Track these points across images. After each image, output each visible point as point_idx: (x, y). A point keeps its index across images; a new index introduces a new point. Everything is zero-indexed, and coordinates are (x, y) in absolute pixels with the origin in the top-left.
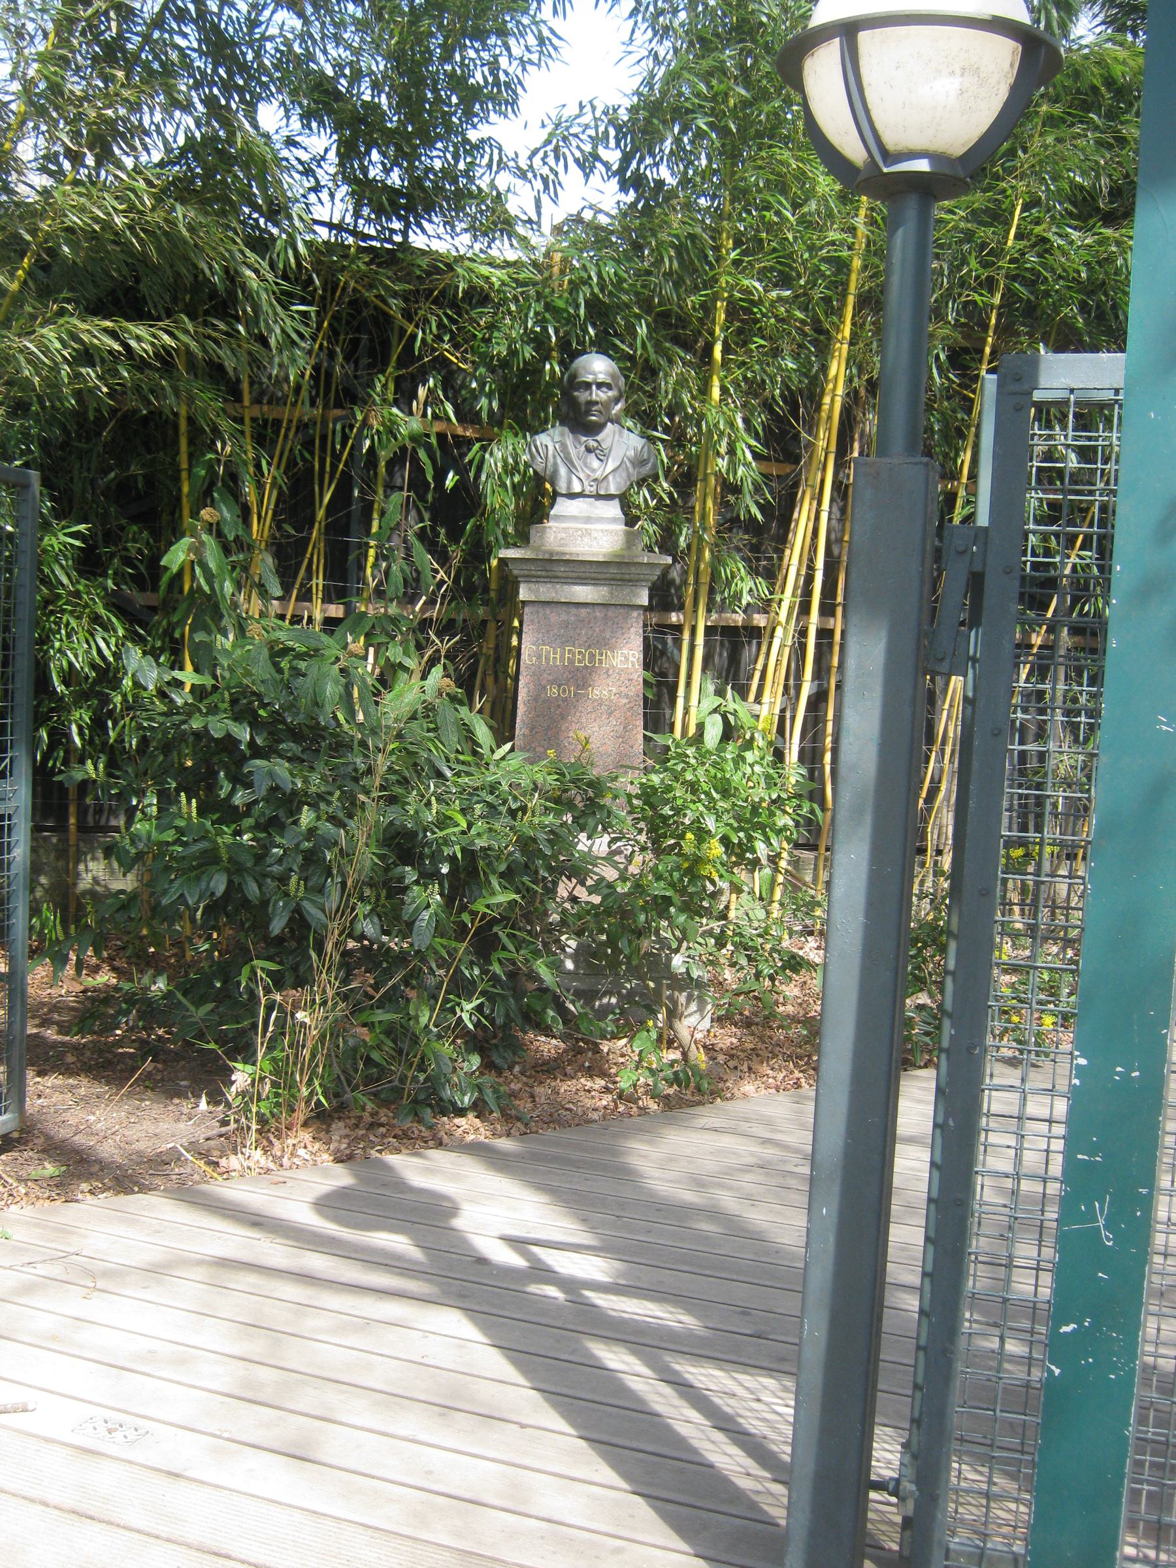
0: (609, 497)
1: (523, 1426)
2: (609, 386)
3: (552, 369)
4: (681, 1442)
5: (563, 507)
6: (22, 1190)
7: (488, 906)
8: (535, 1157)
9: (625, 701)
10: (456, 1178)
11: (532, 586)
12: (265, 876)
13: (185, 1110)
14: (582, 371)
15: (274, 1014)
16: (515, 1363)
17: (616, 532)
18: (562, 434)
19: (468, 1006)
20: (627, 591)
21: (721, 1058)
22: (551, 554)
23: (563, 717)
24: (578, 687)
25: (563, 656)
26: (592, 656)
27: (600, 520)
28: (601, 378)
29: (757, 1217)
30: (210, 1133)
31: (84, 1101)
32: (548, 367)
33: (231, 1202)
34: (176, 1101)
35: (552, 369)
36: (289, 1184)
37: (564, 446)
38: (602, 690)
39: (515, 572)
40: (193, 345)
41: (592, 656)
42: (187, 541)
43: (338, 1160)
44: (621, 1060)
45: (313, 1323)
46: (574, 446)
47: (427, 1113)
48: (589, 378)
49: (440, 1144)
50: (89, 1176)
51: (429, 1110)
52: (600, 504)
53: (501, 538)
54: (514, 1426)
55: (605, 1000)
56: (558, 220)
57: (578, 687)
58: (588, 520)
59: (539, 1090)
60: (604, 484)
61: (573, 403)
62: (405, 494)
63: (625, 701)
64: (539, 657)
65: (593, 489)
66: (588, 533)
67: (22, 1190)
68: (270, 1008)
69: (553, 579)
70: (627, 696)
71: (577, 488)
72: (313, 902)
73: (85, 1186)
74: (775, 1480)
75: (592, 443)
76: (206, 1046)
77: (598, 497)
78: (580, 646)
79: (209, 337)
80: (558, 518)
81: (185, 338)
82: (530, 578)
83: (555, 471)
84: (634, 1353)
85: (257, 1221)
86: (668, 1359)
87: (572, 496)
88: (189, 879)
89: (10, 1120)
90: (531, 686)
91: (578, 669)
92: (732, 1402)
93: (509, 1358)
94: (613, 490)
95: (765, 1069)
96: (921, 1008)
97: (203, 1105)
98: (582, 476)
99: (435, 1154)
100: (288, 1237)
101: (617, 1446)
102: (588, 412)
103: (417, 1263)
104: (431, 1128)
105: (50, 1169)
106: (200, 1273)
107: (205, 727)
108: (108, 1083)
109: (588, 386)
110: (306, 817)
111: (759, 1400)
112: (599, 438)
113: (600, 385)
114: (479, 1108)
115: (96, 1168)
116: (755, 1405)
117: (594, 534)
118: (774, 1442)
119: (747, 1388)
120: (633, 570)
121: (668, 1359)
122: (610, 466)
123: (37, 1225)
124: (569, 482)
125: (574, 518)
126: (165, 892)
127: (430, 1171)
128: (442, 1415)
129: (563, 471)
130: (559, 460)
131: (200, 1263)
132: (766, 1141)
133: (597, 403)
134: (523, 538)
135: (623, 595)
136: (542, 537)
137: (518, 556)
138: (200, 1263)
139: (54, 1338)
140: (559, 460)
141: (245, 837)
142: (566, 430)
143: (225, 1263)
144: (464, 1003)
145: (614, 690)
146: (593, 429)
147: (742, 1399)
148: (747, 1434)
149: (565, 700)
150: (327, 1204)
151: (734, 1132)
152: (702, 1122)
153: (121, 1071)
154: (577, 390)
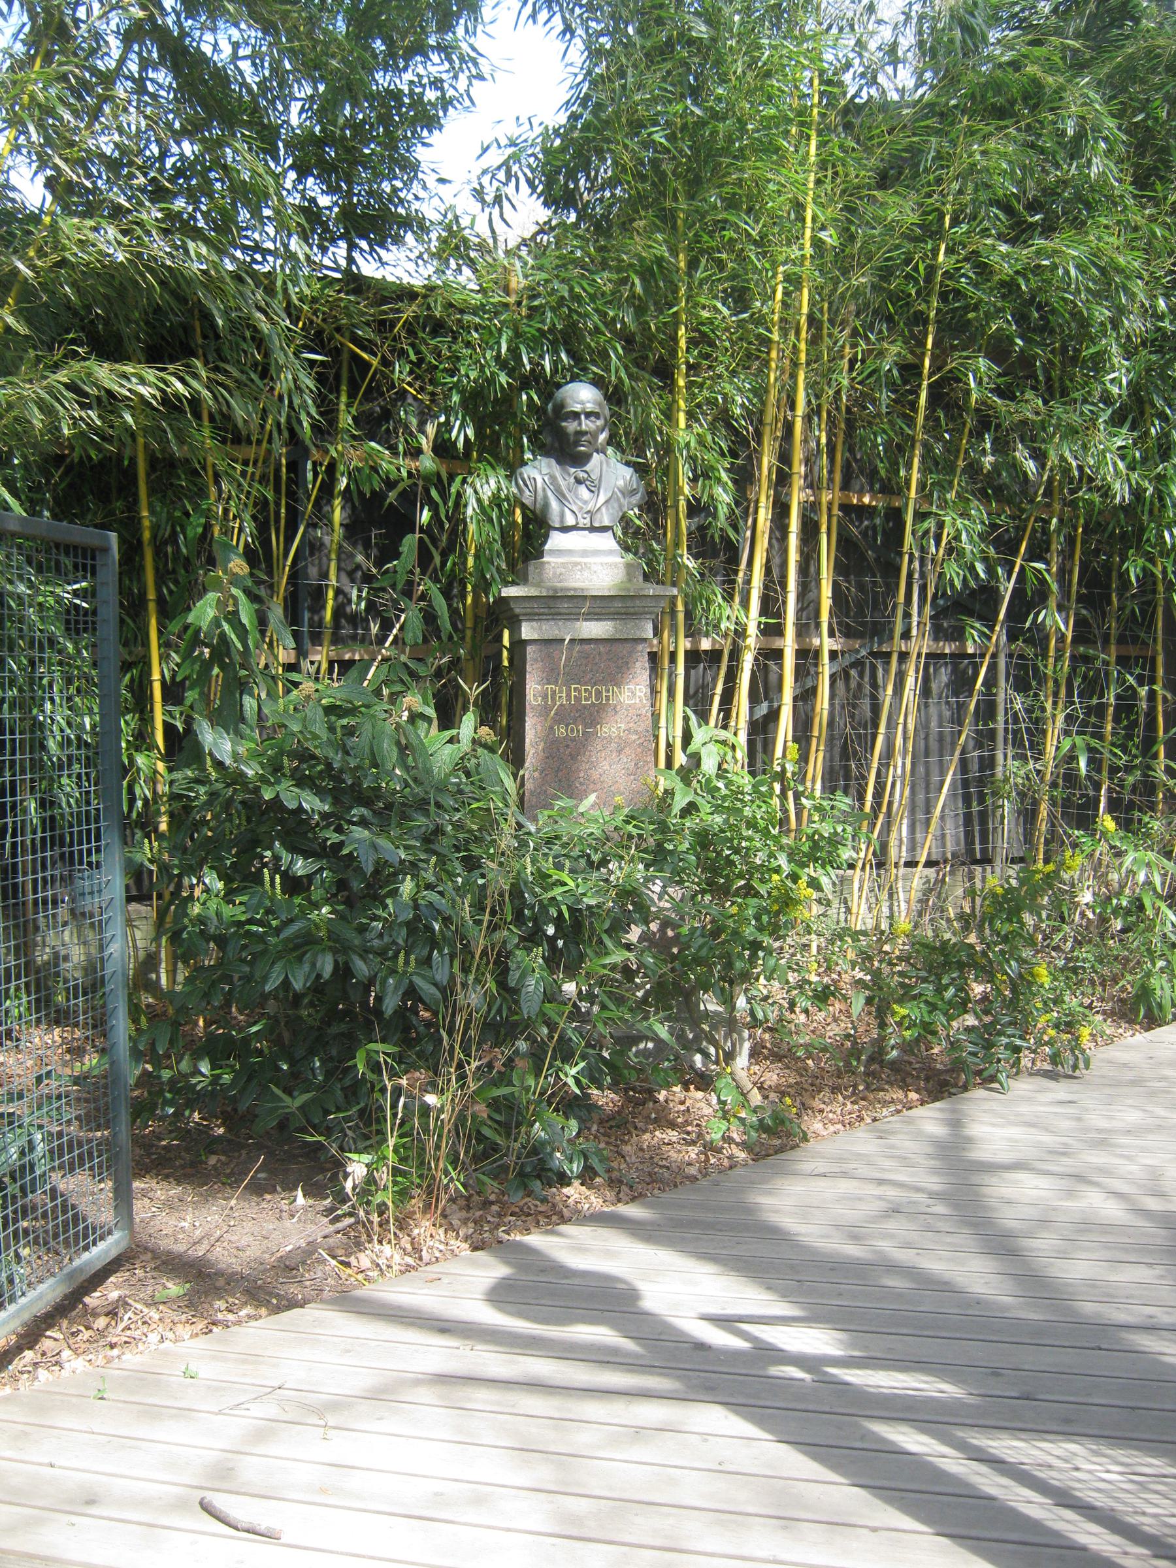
0: (603, 529)
1: (874, 1530)
2: (597, 415)
3: (530, 398)
4: (1035, 1526)
5: (556, 540)
6: (156, 1316)
7: (604, 966)
8: (679, 1224)
9: (634, 737)
10: (610, 1254)
11: (534, 624)
12: (367, 951)
13: (286, 1208)
14: (569, 401)
15: (402, 1100)
16: (815, 1457)
17: (616, 565)
18: (549, 466)
19: (574, 1071)
20: (631, 624)
21: (773, 1096)
22: (555, 590)
23: (573, 757)
24: (586, 727)
25: (568, 696)
26: (599, 693)
27: (596, 553)
28: (590, 407)
29: (936, 1264)
30: (327, 1231)
31: (169, 1206)
32: (524, 397)
33: (399, 1308)
34: (268, 1197)
35: (530, 398)
36: (445, 1280)
37: (553, 478)
38: (612, 728)
39: (517, 611)
40: (206, 393)
41: (599, 693)
42: (212, 596)
43: (475, 1248)
44: (682, 1108)
45: (583, 1438)
46: (564, 477)
47: (537, 1185)
48: (577, 408)
49: (564, 1220)
50: (219, 1293)
51: (538, 1183)
52: (595, 536)
53: (496, 576)
54: (865, 1531)
55: (642, 1046)
56: (511, 244)
57: (586, 727)
58: (585, 553)
59: (627, 1149)
60: (598, 515)
61: (561, 434)
62: (417, 536)
63: (634, 737)
64: (545, 697)
65: (587, 521)
66: (587, 566)
67: (156, 1316)
68: (397, 1091)
69: (555, 616)
70: (636, 732)
71: (570, 520)
72: (424, 977)
73: (220, 1304)
74: (1156, 1556)
75: (582, 475)
76: (310, 1139)
77: (593, 529)
78: (585, 684)
79: (222, 385)
80: (552, 552)
81: (195, 384)
82: (532, 617)
83: (546, 505)
84: (924, 1431)
85: (444, 1327)
86: (960, 1434)
87: (565, 529)
88: (289, 961)
89: (121, 1238)
90: (539, 727)
91: (585, 706)
92: (1054, 1474)
93: (806, 1453)
94: (606, 523)
95: (817, 1104)
96: (969, 1030)
97: (301, 1200)
98: (574, 508)
99: (563, 1228)
100: (487, 1342)
101: (978, 1539)
102: (577, 443)
103: (637, 1356)
104: (544, 1200)
105: (174, 1288)
106: (425, 1394)
107: (277, 796)
108: (179, 1183)
109: (576, 415)
110: (407, 887)
111: (1077, 1469)
112: (587, 468)
113: (588, 415)
114: (587, 1176)
115: (221, 1282)
116: (1076, 1474)
117: (594, 568)
118: (1126, 1513)
119: (1058, 1457)
120: (638, 603)
121: (960, 1434)
122: (602, 498)
123: (214, 1358)
124: (562, 516)
125: (570, 552)
126: (265, 979)
127: (580, 1249)
128: (785, 1528)
129: (554, 505)
130: (549, 493)
131: (417, 1383)
132: (881, 1182)
133: (586, 433)
134: (520, 578)
135: (630, 630)
136: (540, 574)
137: (521, 594)
138: (417, 1383)
139: (323, 1491)
140: (549, 493)
141: (324, 910)
142: (553, 462)
143: (443, 1379)
144: (567, 1067)
145: (623, 726)
146: (580, 460)
147: (1060, 1470)
148: (1093, 1508)
149: (573, 740)
150: (500, 1295)
151: (845, 1175)
152: (807, 1167)
153: (183, 1167)
154: (565, 420)
